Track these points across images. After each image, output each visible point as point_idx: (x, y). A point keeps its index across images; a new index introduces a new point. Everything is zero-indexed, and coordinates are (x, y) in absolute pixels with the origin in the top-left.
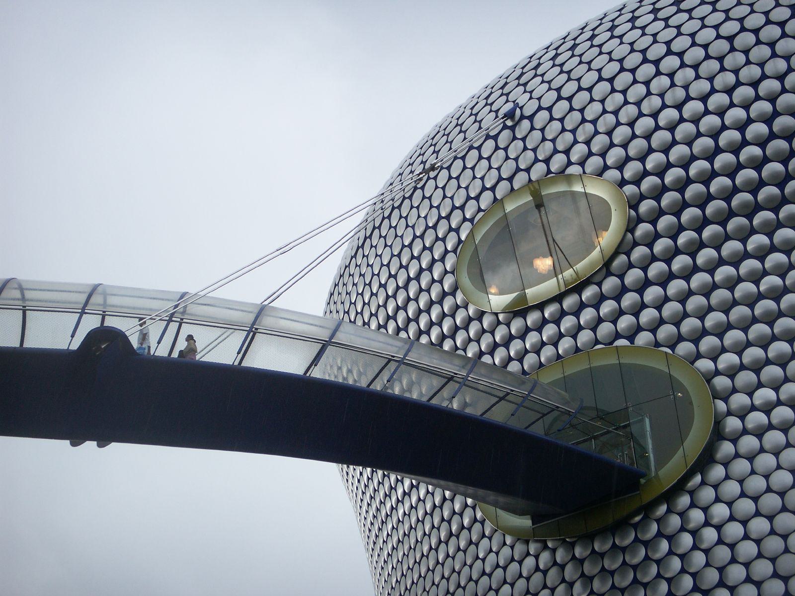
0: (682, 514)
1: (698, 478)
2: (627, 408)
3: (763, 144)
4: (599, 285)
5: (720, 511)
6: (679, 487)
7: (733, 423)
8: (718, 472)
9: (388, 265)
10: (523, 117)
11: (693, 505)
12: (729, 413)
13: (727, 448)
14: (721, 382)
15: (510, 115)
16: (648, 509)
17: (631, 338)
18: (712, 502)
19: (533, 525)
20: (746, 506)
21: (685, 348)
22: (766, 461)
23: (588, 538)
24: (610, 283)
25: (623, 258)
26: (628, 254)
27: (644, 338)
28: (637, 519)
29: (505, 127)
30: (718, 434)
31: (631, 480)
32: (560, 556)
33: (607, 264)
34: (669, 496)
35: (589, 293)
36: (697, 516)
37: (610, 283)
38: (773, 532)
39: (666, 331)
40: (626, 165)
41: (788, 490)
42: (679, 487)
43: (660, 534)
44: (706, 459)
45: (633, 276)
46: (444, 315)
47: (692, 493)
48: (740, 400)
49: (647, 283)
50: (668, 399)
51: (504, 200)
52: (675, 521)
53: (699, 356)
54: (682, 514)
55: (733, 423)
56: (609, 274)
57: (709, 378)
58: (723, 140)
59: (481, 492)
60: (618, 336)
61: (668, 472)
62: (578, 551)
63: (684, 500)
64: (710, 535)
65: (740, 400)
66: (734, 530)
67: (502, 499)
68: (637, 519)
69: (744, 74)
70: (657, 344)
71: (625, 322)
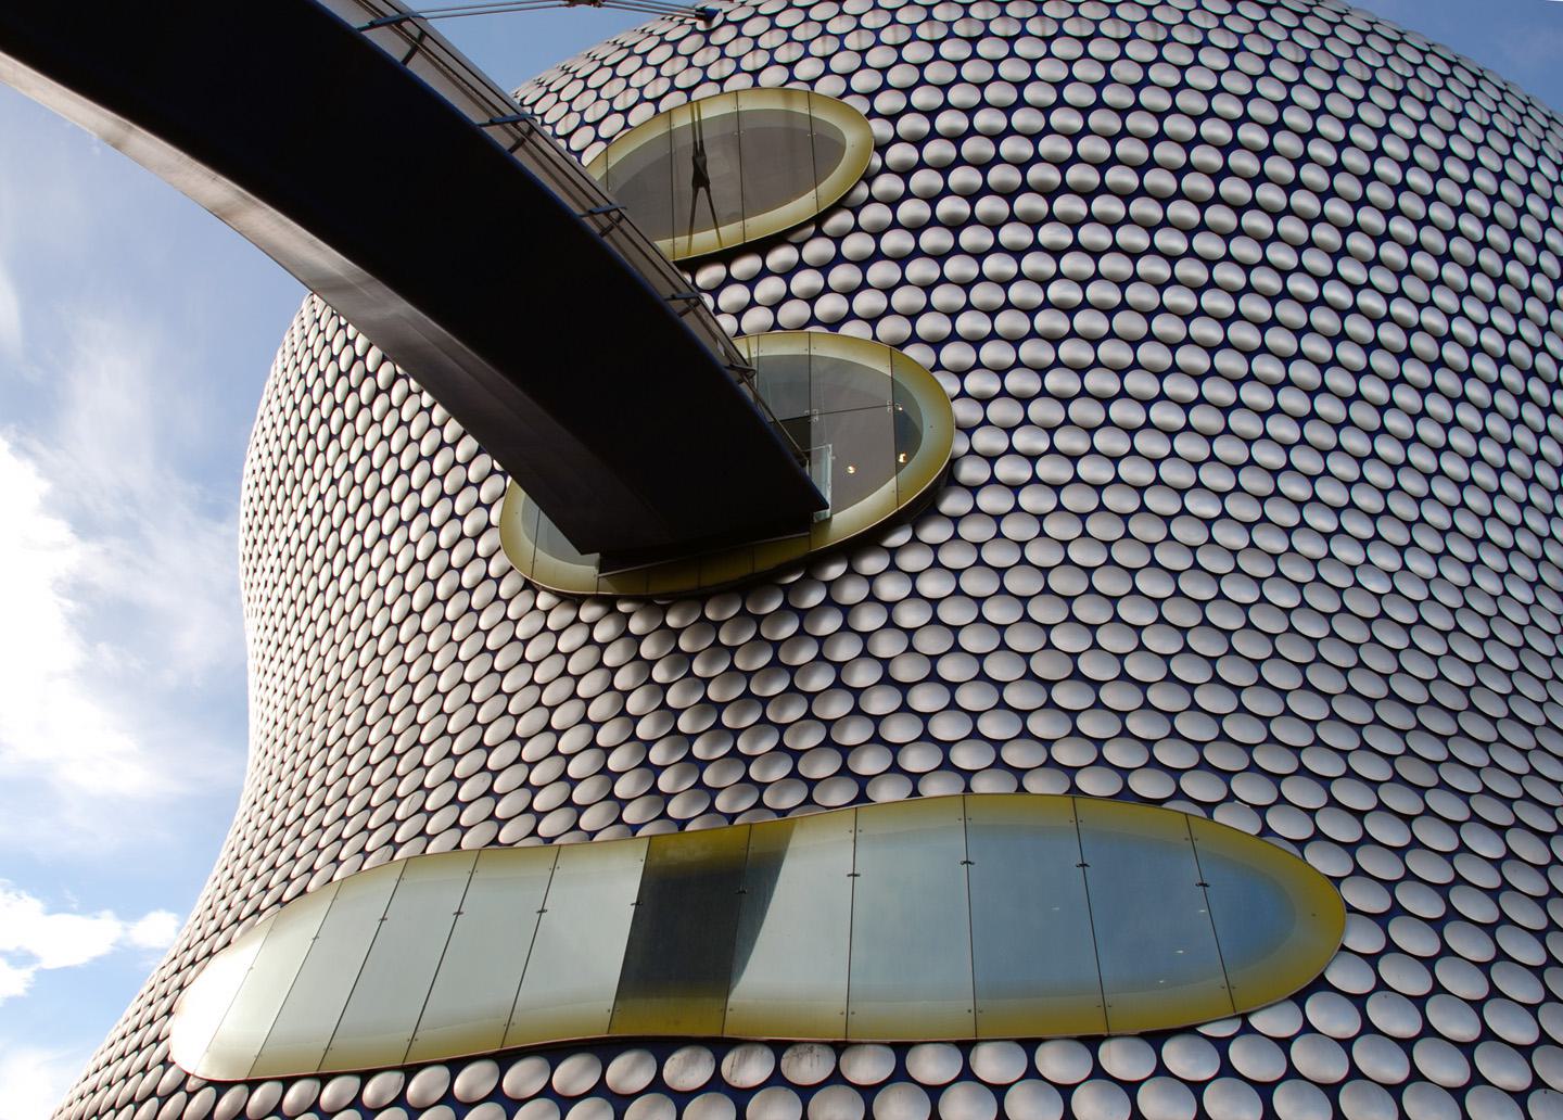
2: (809, 417)
4: (800, 246)
8: (934, 532)
9: (362, 485)
13: (954, 503)
16: (812, 565)
18: (1091, 516)
19: (600, 572)
24: (819, 249)
26: (856, 211)
28: (793, 579)
29: (694, 31)
30: (949, 479)
33: (819, 219)
35: (782, 256)
37: (819, 249)
41: (993, 595)
42: (871, 539)
44: (921, 510)
45: (856, 245)
48: (985, 440)
51: (674, 114)
55: (971, 471)
56: (819, 233)
58: (1030, 93)
62: (636, 625)
63: (872, 564)
68: (793, 579)
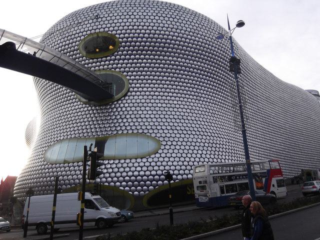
0: (119, 104)
1: (123, 98)
3: (147, 38)
5: (126, 105)
6: (120, 99)
7: (131, 89)
8: (127, 98)
10: (100, 17)
11: (122, 103)
12: (131, 87)
13: (129, 94)
14: (131, 81)
15: (97, 16)
16: (113, 103)
17: (115, 69)
20: (131, 105)
21: (125, 73)
22: (136, 97)
23: (100, 106)
25: (116, 53)
27: (118, 70)
30: (129, 91)
31: (112, 96)
32: (93, 108)
34: (117, 101)
36: (122, 105)
38: (144, 122)
39: (122, 69)
40: (281, 81)
43: (115, 107)
44: (126, 95)
46: (64, 101)
47: (122, 101)
48: (133, 85)
49: (120, 59)
50: (121, 85)
52: (118, 105)
53: (128, 76)
54: (119, 104)
55: (131, 89)
56: (113, 56)
57: (129, 80)
59: (77, 92)
60: (113, 68)
61: (116, 97)
63: (120, 102)
64: (124, 109)
65: (133, 85)
66: (129, 109)
67: (81, 94)
69: (131, 24)
70: (120, 72)
71: (115, 66)
